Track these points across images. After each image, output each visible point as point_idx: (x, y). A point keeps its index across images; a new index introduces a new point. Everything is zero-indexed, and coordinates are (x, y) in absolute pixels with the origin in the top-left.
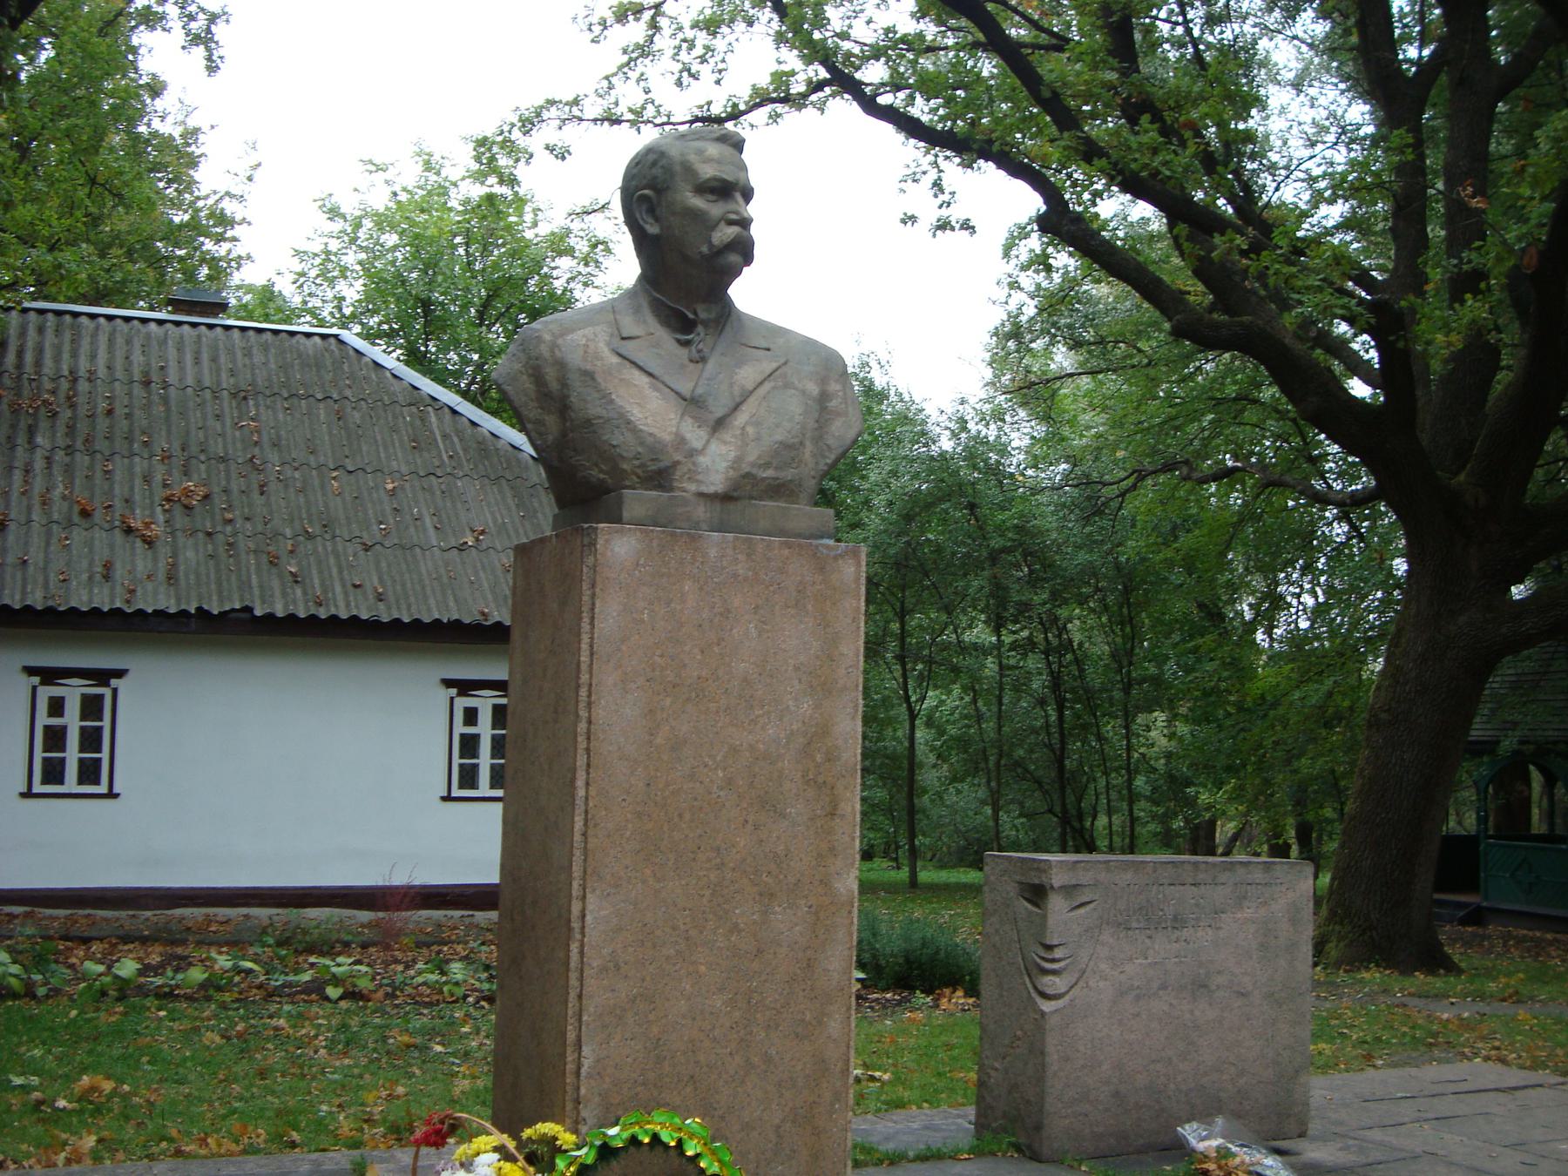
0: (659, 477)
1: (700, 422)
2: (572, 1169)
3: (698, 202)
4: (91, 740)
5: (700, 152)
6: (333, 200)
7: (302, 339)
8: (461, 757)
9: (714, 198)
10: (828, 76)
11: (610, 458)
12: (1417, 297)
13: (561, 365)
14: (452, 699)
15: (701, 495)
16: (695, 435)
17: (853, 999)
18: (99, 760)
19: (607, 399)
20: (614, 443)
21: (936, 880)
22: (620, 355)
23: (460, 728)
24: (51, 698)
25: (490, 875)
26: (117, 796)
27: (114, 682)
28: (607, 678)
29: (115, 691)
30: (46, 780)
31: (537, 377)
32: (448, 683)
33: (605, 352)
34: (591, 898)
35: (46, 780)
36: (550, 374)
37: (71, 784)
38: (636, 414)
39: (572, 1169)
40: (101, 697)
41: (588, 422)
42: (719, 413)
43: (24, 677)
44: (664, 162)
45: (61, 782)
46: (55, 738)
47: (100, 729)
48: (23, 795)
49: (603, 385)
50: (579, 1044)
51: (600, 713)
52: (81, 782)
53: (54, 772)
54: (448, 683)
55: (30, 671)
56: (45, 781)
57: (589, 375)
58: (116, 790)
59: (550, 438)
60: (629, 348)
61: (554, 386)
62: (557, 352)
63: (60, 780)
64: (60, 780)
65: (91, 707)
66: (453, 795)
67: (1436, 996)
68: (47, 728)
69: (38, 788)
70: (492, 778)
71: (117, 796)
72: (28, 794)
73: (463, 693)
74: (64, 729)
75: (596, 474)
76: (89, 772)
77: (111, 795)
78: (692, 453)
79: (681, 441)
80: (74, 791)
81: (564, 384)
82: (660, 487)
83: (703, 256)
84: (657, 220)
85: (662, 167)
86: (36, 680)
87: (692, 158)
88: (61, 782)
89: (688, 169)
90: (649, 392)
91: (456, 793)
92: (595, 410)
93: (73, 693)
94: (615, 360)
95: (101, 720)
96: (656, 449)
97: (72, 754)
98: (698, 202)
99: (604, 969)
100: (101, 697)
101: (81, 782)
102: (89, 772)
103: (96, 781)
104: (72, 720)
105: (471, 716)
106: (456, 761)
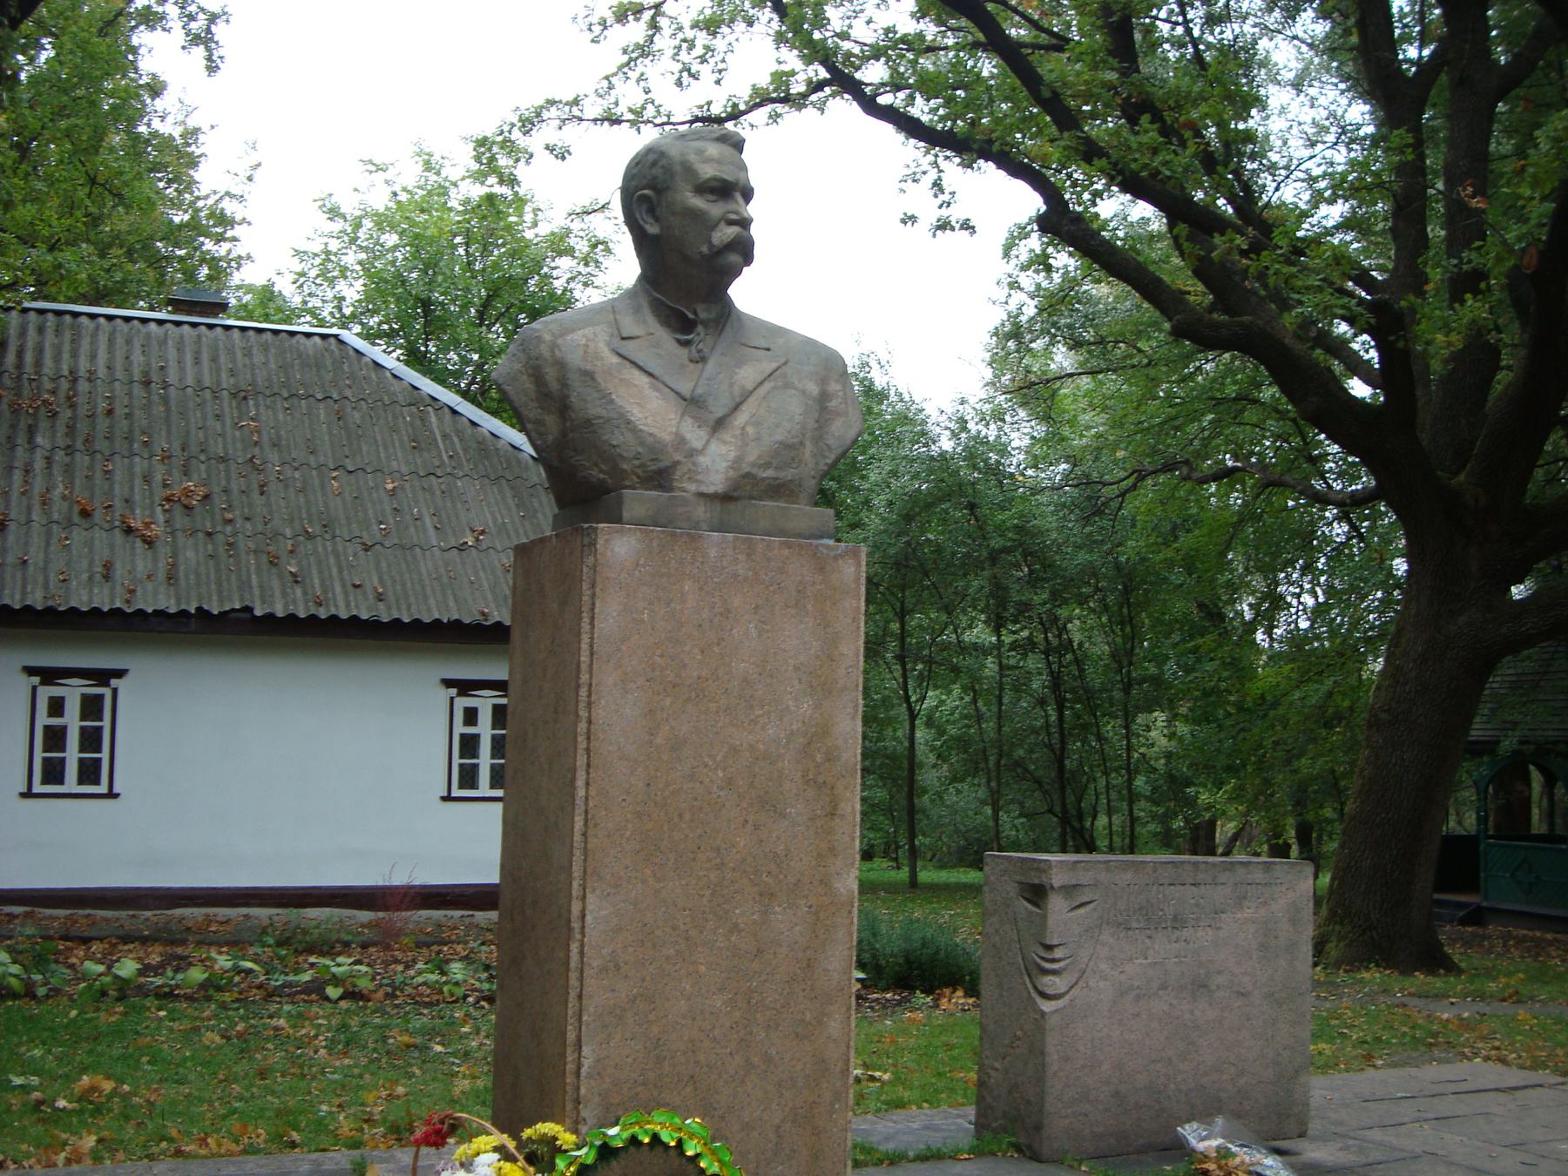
0: (659, 477)
1: (700, 422)
2: (572, 1169)
3: (698, 202)
4: (91, 740)
5: (700, 152)
6: (333, 200)
7: (302, 339)
8: (461, 757)
9: (714, 198)
10: (828, 76)
11: (610, 458)
12: (1417, 297)
13: (561, 365)
14: (452, 699)
15: (701, 495)
16: (695, 435)
17: (853, 999)
18: (99, 760)
19: (607, 399)
20: (614, 443)
21: (936, 880)
22: (620, 355)
23: (460, 728)
24: (51, 698)
25: (490, 875)
26: (117, 796)
27: (114, 682)
28: (607, 678)
29: (115, 691)
30: (46, 780)
31: (537, 377)
32: (448, 683)
33: (605, 352)
34: (591, 898)
35: (46, 780)
36: (550, 374)
37: (71, 784)
38: (636, 414)
39: (572, 1169)
40: (101, 697)
41: (588, 422)
42: (719, 413)
43: (24, 677)
44: (664, 162)
45: (61, 782)
46: (55, 738)
47: (100, 729)
48: (23, 795)
49: (603, 385)
50: (579, 1044)
51: (600, 713)
52: (81, 782)
53: (54, 772)
54: (448, 683)
55: (30, 671)
56: (45, 781)
57: (589, 375)
58: (116, 790)
59: (550, 438)
60: (629, 348)
61: (554, 386)
62: (557, 352)
63: (60, 780)
64: (60, 780)
65: (91, 707)
66: (453, 795)
67: (1436, 996)
68: (47, 728)
69: (38, 788)
70: (492, 778)
71: (117, 796)
72: (28, 794)
73: (463, 693)
74: (64, 729)
75: (596, 474)
76: (89, 772)
77: (111, 795)
78: (692, 453)
79: (681, 441)
80: (74, 791)
81: (564, 384)
82: (660, 487)
83: (703, 256)
84: (657, 220)
85: (662, 167)
86: (36, 680)
87: (692, 158)
88: (61, 782)
89: (688, 169)
90: (649, 392)
91: (456, 793)
92: (595, 410)
93: (73, 693)
94: (615, 360)
95: (101, 720)
96: (656, 449)
97: (72, 754)
98: (698, 202)
99: (604, 969)
100: (101, 697)
101: (81, 782)
102: (89, 772)
103: (96, 781)
104: (72, 720)
105: (471, 716)
106: (456, 761)
